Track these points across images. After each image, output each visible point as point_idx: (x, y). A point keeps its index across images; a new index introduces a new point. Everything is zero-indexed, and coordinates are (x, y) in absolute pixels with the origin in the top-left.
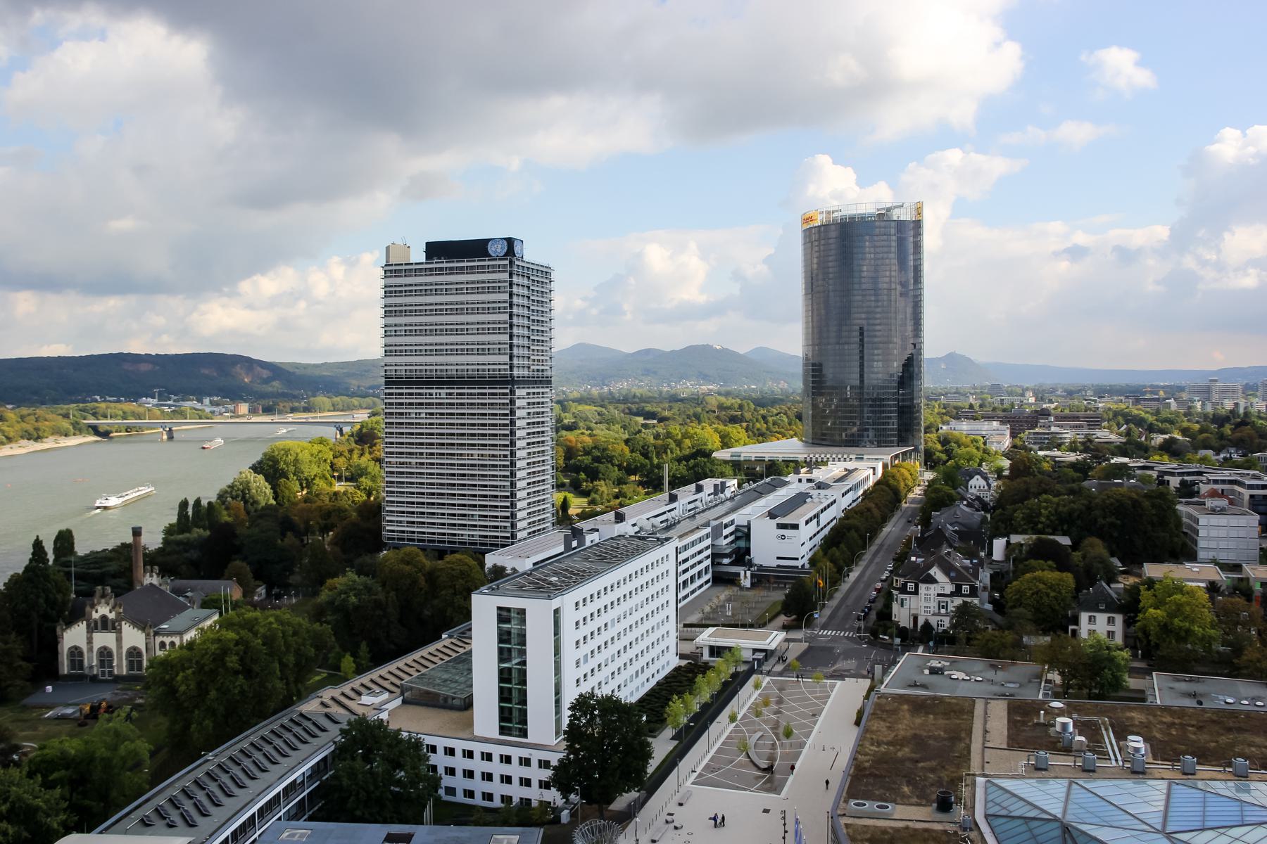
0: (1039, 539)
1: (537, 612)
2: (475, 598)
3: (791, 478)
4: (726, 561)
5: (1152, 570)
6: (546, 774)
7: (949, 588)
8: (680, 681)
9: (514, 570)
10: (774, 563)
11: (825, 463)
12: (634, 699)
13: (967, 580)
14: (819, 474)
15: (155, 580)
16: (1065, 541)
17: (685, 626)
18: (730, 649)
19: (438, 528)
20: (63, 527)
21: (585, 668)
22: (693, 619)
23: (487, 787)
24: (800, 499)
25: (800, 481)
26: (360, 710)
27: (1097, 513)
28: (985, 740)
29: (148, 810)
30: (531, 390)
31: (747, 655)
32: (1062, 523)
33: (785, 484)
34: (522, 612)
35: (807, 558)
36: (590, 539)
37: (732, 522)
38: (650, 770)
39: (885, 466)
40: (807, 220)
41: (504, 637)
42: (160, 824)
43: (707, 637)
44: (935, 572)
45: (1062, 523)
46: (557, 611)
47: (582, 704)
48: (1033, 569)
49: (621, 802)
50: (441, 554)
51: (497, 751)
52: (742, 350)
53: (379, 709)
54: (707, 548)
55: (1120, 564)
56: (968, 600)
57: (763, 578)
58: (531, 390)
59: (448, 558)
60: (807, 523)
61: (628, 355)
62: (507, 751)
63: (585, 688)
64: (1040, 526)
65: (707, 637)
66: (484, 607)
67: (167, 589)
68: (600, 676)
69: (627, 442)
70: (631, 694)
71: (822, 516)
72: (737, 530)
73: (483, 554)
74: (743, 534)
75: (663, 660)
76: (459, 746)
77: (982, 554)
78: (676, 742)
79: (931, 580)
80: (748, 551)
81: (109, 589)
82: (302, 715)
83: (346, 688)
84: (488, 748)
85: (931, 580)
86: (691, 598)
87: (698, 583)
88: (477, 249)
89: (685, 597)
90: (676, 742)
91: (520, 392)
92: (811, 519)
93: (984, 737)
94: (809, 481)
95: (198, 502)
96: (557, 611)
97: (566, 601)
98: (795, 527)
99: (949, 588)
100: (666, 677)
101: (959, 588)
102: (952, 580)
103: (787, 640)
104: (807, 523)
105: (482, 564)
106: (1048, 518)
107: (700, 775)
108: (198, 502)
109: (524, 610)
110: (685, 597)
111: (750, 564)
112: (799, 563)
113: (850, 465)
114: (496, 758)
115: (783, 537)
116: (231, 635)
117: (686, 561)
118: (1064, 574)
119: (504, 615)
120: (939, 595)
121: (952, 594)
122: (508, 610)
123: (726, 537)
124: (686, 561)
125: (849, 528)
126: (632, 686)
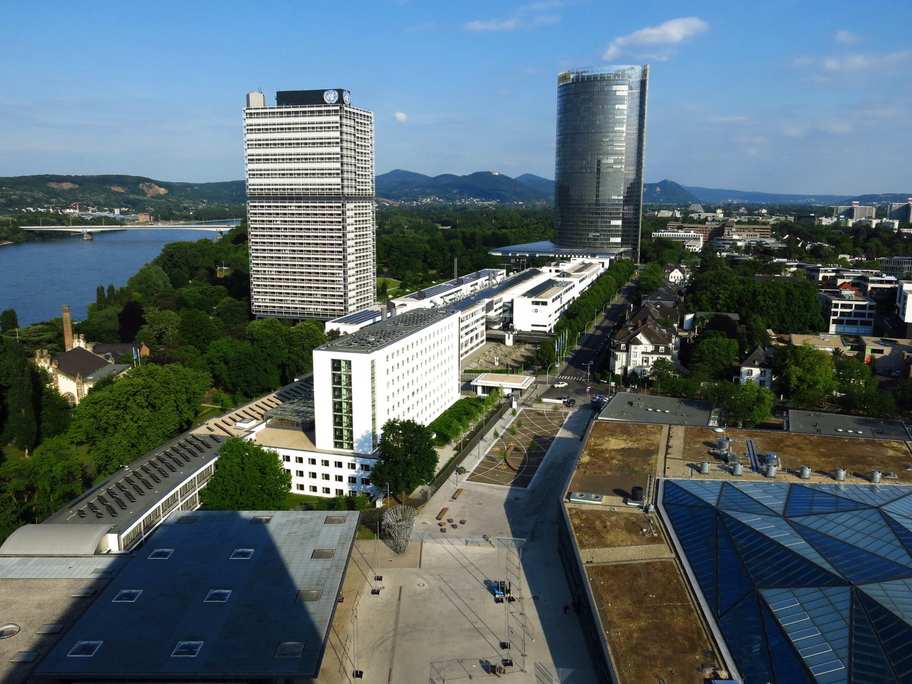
0: (716, 316)
1: (360, 362)
2: (316, 353)
3: (545, 269)
4: (496, 327)
5: (798, 340)
6: (367, 475)
7: (651, 348)
8: (458, 414)
9: (345, 333)
10: (529, 329)
11: (569, 260)
12: (427, 424)
13: (663, 343)
14: (565, 267)
15: (82, 344)
16: (735, 317)
17: (466, 371)
18: (497, 388)
19: (291, 303)
20: (7, 308)
21: (393, 402)
22: (474, 366)
23: (326, 484)
24: (549, 284)
25: (550, 271)
26: (235, 433)
27: (760, 298)
28: (667, 453)
29: (83, 506)
30: (357, 204)
31: (507, 392)
32: (737, 304)
33: (538, 273)
34: (349, 363)
35: (552, 326)
36: (399, 311)
37: (501, 300)
38: (437, 471)
39: (611, 261)
40: (564, 78)
41: (336, 380)
42: (90, 515)
43: (481, 381)
44: (640, 337)
45: (737, 304)
46: (373, 362)
47: (390, 427)
48: (711, 337)
49: (418, 491)
50: (295, 321)
51: (332, 459)
52: (513, 175)
53: (250, 432)
54: (482, 318)
55: (773, 334)
56: (663, 356)
57: (520, 339)
58: (357, 204)
59: (299, 325)
60: (553, 301)
61: (430, 179)
62: (339, 459)
63: (392, 416)
64: (719, 306)
65: (481, 381)
66: (322, 360)
67: (89, 349)
68: (404, 407)
69: (429, 242)
70: (425, 417)
71: (563, 296)
72: (504, 306)
73: (324, 322)
74: (509, 308)
75: (448, 396)
76: (306, 456)
77: (676, 325)
78: (455, 452)
79: (638, 343)
80: (511, 321)
81: (45, 352)
82: (193, 436)
83: (226, 418)
84: (326, 457)
85: (638, 343)
86: (476, 349)
87: (475, 342)
88: (314, 98)
89: (466, 352)
90: (455, 452)
91: (350, 206)
92: (556, 299)
93: (667, 450)
94: (557, 271)
95: (111, 288)
96: (373, 362)
97: (379, 355)
98: (545, 303)
99: (651, 348)
100: (450, 409)
101: (657, 349)
102: (652, 343)
103: (535, 382)
104: (553, 301)
105: (323, 327)
106: (724, 301)
107: (473, 474)
108: (111, 288)
109: (350, 362)
110: (466, 352)
111: (512, 329)
112: (547, 329)
113: (587, 260)
114: (332, 464)
115: (536, 311)
116: (140, 380)
117: (467, 327)
118: (732, 340)
119: (336, 365)
120: (643, 353)
121: (652, 353)
122: (339, 361)
123: (496, 310)
124: (467, 327)
125: (583, 306)
126: (426, 414)
